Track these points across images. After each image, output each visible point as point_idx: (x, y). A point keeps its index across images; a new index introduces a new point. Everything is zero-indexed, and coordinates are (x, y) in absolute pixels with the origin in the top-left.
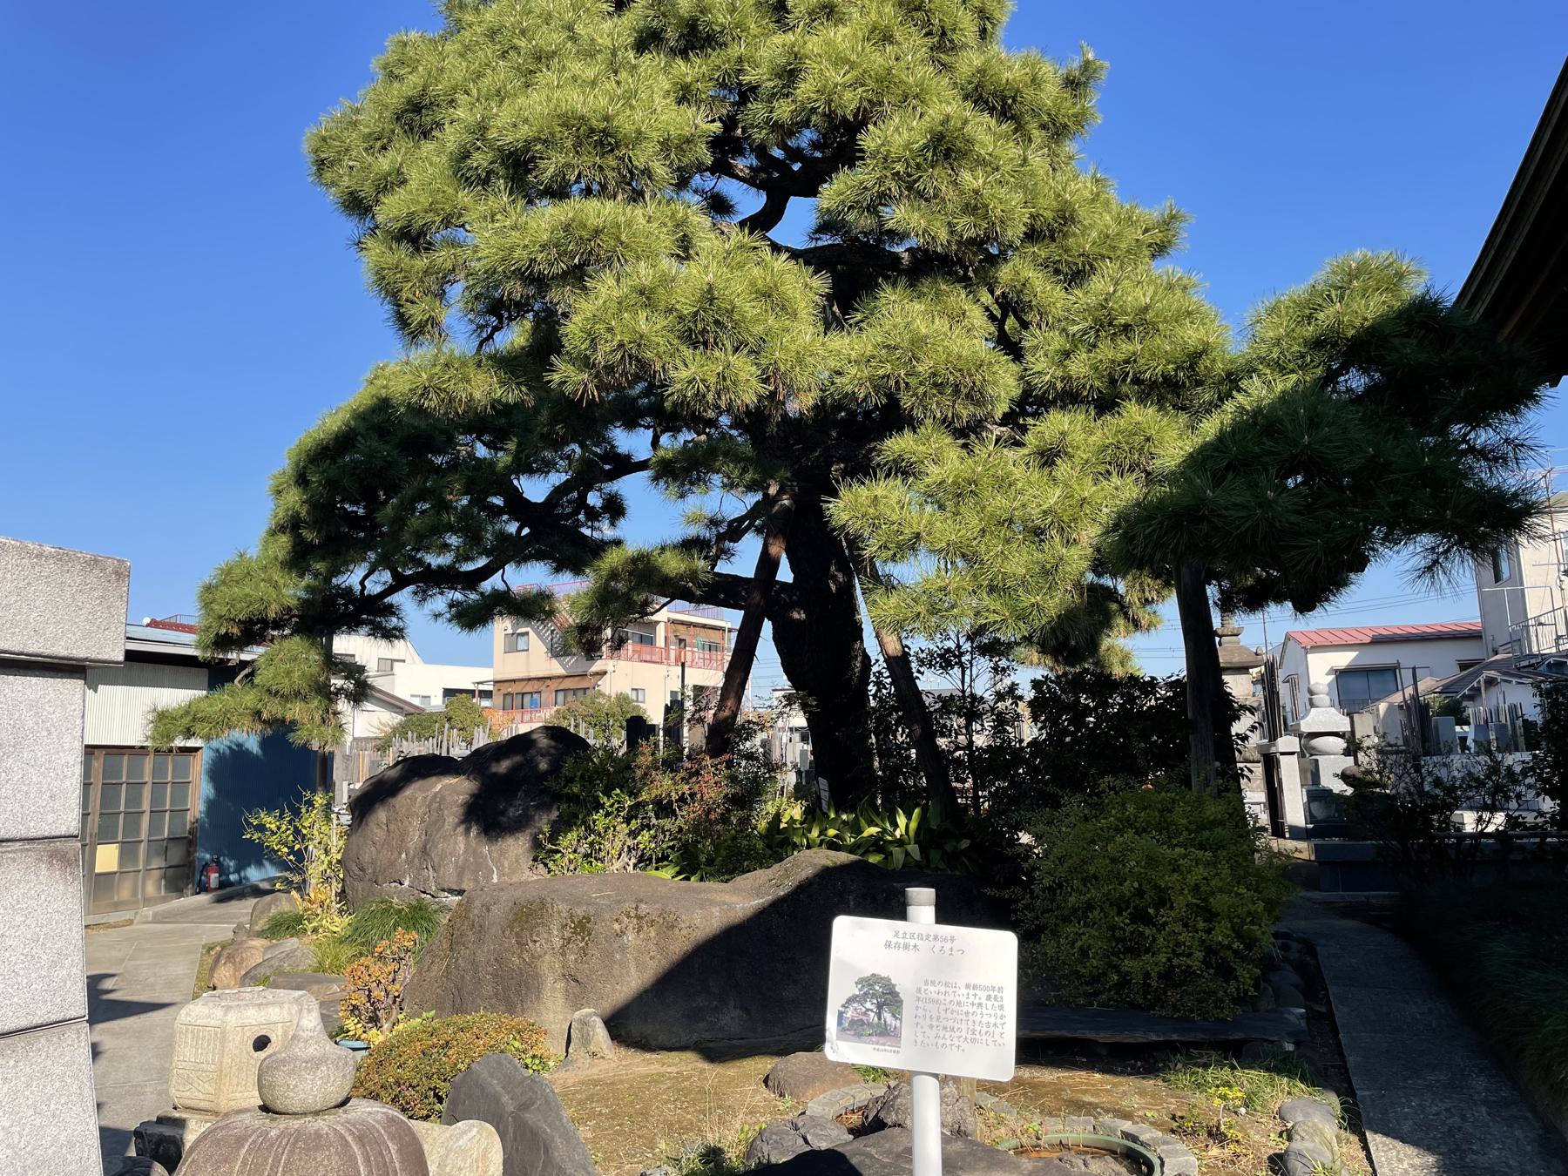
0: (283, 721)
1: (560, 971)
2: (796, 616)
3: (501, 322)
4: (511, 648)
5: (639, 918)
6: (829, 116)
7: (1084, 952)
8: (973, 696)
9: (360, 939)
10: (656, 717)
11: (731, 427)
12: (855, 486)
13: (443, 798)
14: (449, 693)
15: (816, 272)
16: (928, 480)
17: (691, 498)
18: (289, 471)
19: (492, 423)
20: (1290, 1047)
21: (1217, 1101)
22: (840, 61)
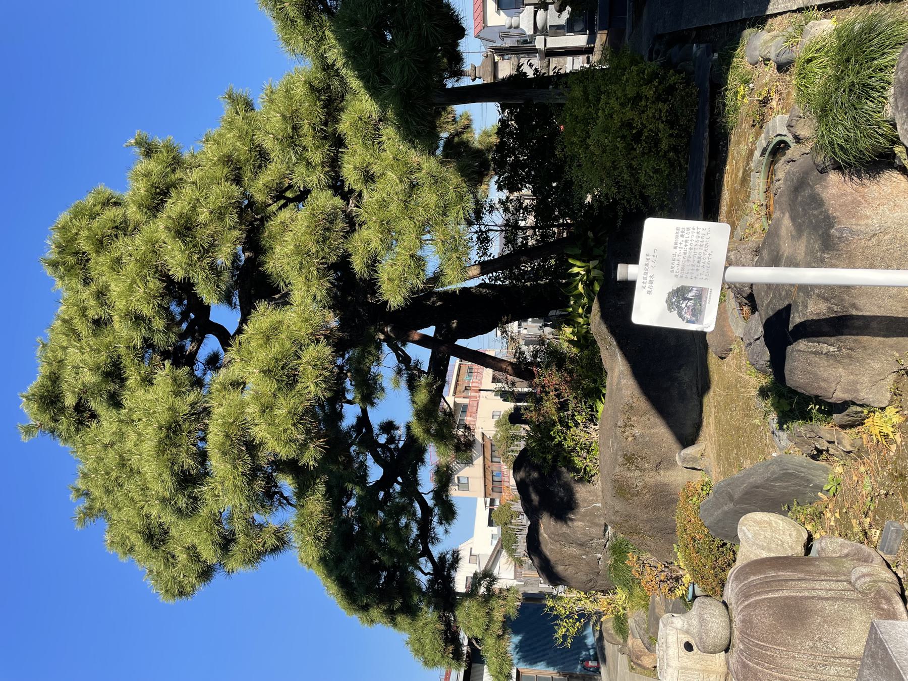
0: (503, 622)
1: (654, 472)
2: (455, 325)
3: (277, 493)
4: (465, 487)
5: (625, 426)
6: (163, 297)
7: (656, 171)
8: (505, 225)
9: (629, 584)
10: (509, 406)
11: (344, 358)
12: (381, 291)
13: (552, 533)
14: (490, 524)
15: (255, 308)
16: (380, 248)
17: (384, 385)
18: (360, 615)
19: (336, 496)
20: (716, 55)
21: (745, 101)
22: (131, 289)
